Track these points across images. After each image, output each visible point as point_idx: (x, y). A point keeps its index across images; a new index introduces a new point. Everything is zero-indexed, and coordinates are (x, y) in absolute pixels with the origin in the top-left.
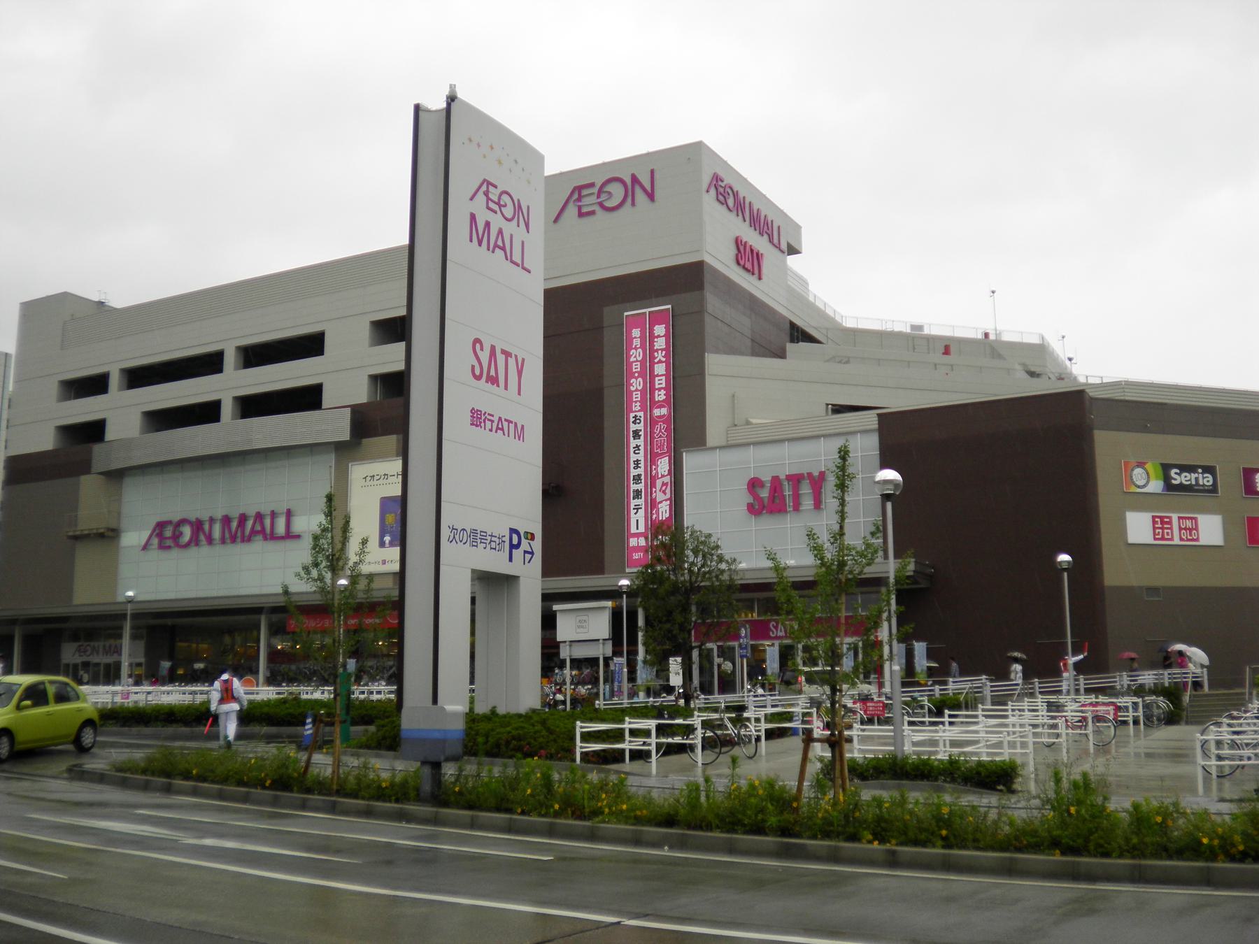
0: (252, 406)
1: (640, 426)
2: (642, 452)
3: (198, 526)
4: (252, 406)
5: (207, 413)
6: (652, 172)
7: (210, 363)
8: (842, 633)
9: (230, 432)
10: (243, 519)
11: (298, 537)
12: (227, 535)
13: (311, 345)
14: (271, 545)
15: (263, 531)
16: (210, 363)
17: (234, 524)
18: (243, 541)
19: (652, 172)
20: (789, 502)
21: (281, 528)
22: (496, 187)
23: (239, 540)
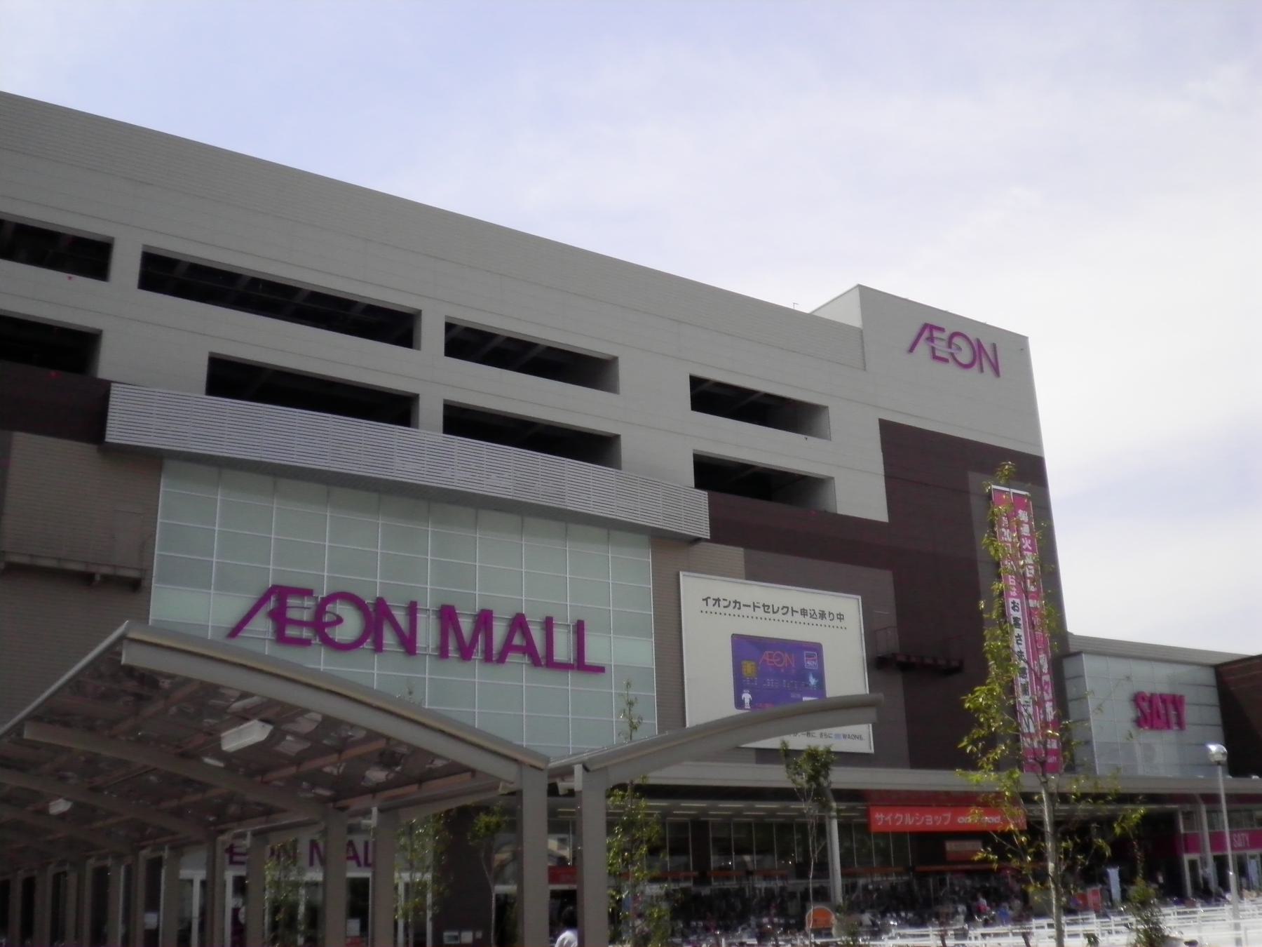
0: (464, 421)
1: (1018, 614)
2: (1023, 643)
3: (376, 616)
4: (464, 421)
5: (395, 408)
6: (911, 350)
7: (395, 327)
8: (773, 911)
9: (421, 454)
10: (484, 620)
11: (599, 669)
12: (452, 645)
13: (586, 370)
14: (547, 680)
15: (529, 649)
16: (395, 327)
17: (466, 625)
18: (488, 658)
19: (911, 350)
20: (1173, 719)
21: (563, 649)
22: (941, 330)
23: (478, 655)
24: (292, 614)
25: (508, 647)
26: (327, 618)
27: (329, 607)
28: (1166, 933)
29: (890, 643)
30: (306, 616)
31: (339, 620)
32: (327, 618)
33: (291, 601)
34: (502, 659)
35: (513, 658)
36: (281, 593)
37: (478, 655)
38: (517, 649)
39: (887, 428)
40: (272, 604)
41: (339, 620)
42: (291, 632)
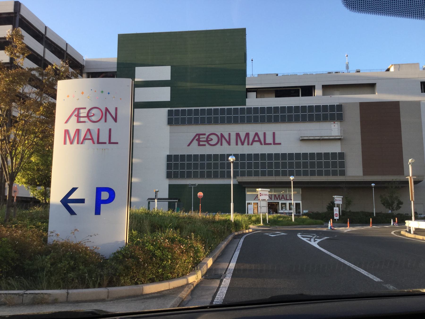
15: (259, 141)
23: (246, 143)
24: (81, 115)
25: (254, 141)
26: (209, 139)
27: (210, 137)
28: (75, 242)
29: (274, 95)
30: (205, 139)
31: (212, 140)
32: (209, 139)
33: (201, 136)
34: (252, 144)
35: (255, 143)
36: (199, 135)
37: (246, 143)
38: (257, 141)
39: (376, 84)
40: (76, 113)
41: (212, 140)
42: (201, 143)
